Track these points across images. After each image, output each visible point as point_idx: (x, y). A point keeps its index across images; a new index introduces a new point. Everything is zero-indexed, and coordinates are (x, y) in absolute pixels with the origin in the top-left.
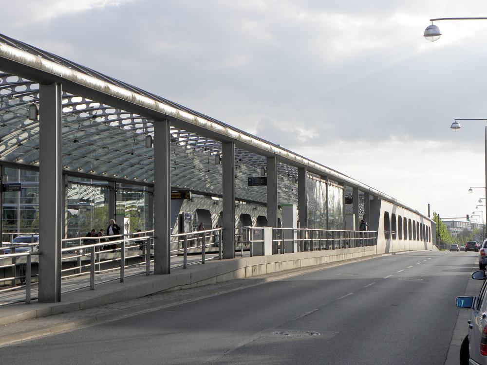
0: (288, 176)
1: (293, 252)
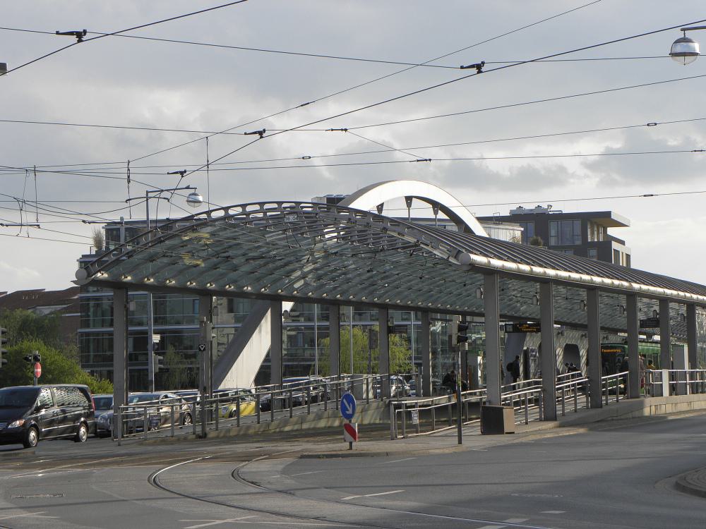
0: (465, 285)
1: (686, 394)
